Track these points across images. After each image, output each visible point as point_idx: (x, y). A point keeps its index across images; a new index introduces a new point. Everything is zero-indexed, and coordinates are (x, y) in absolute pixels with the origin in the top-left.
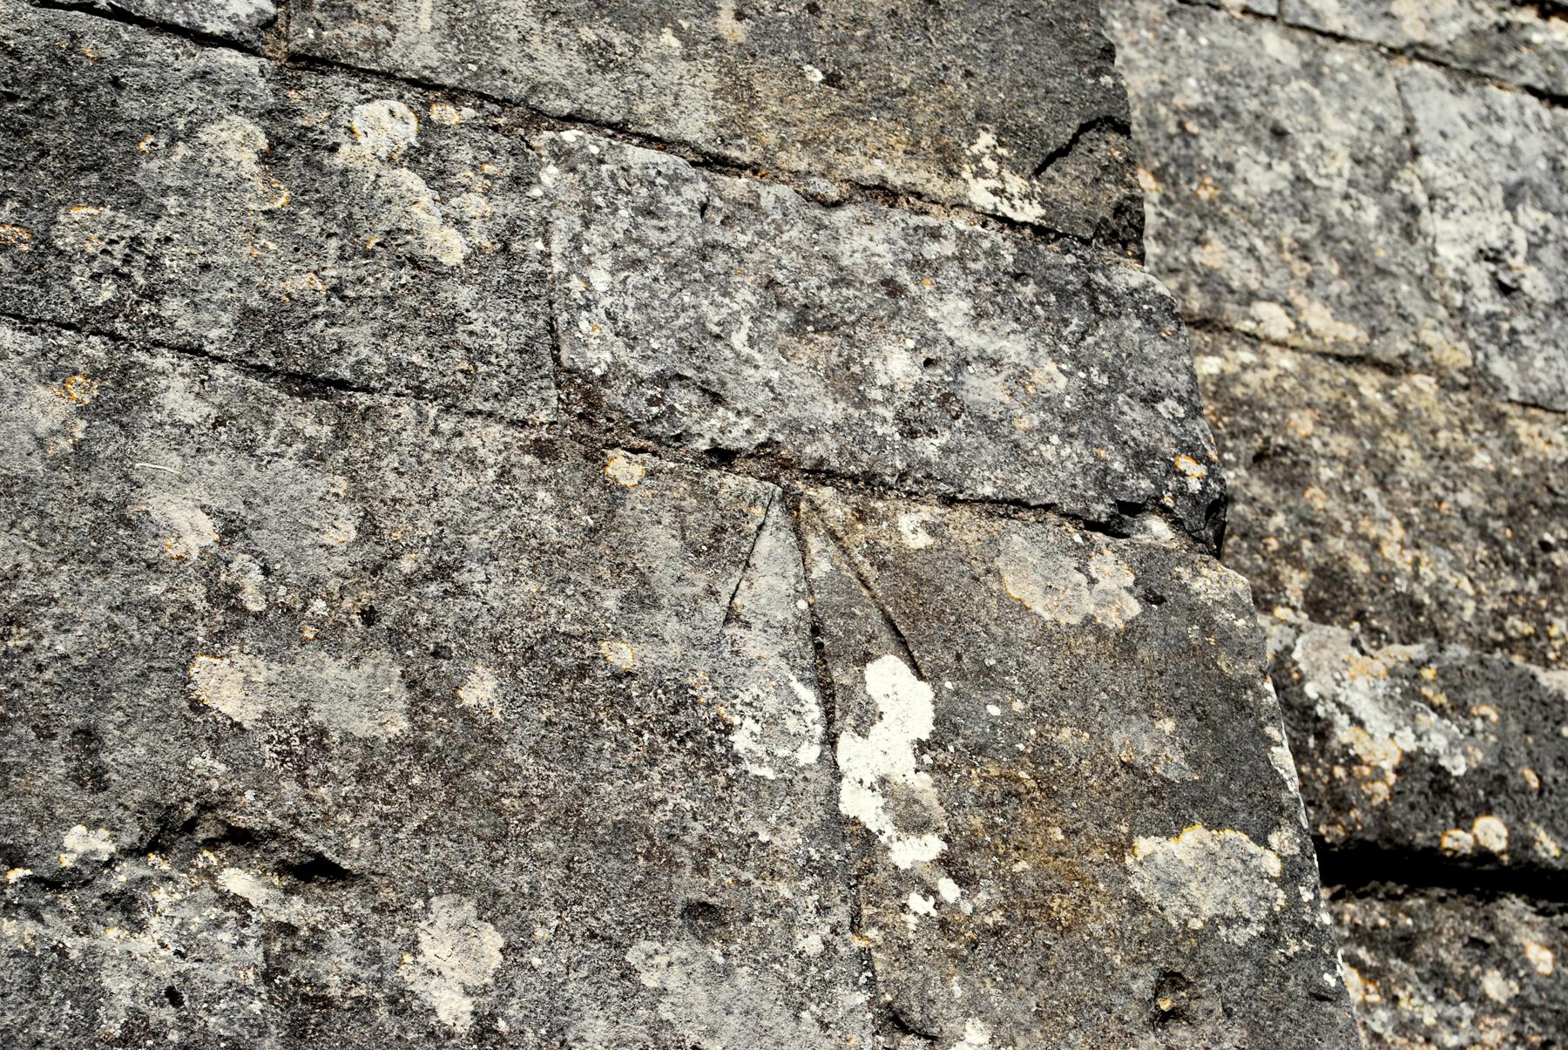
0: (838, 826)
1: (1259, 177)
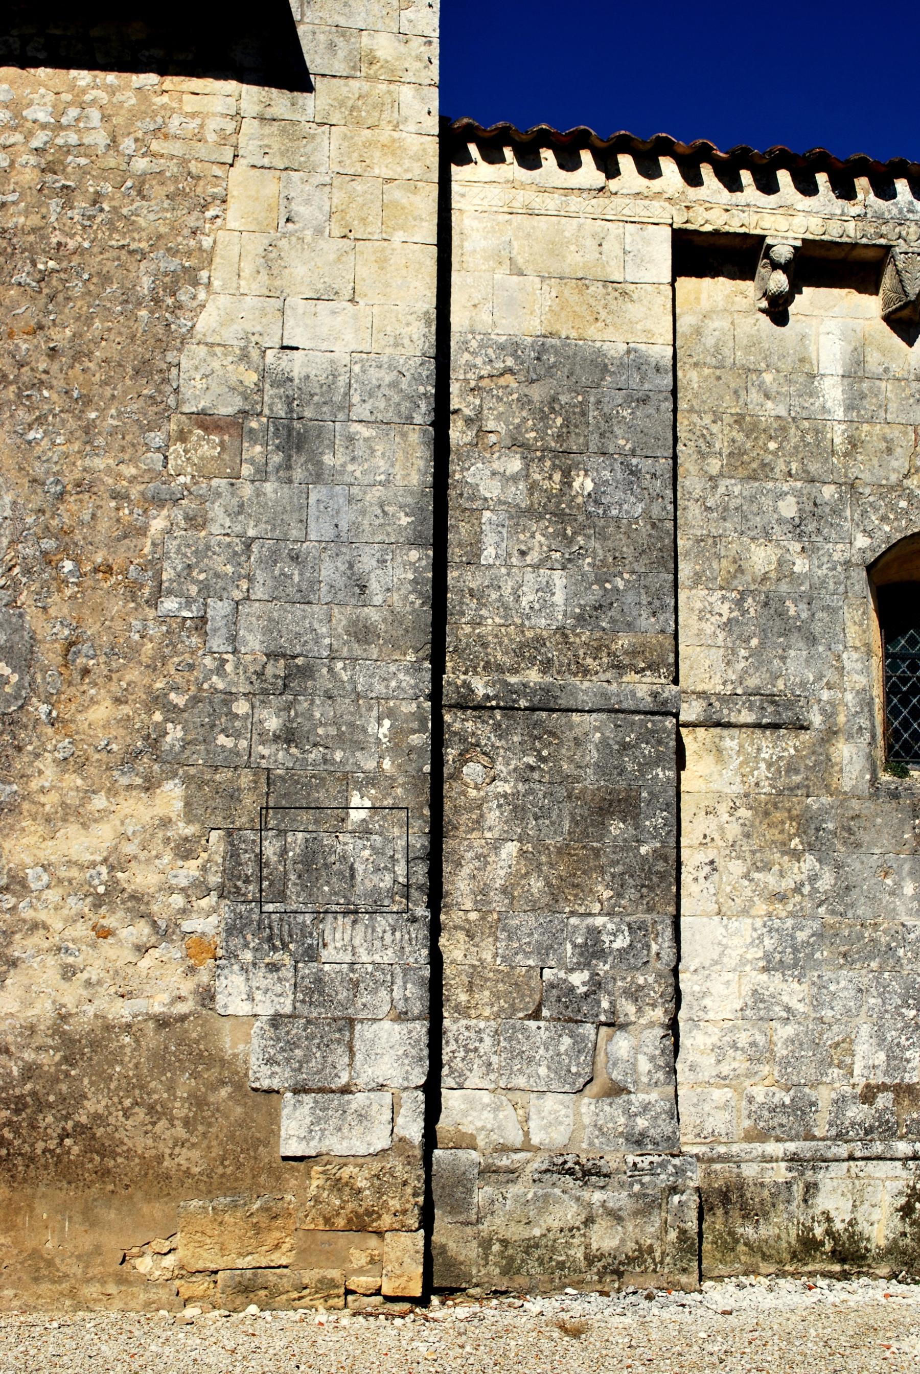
0: (378, 738)
1: (494, 595)
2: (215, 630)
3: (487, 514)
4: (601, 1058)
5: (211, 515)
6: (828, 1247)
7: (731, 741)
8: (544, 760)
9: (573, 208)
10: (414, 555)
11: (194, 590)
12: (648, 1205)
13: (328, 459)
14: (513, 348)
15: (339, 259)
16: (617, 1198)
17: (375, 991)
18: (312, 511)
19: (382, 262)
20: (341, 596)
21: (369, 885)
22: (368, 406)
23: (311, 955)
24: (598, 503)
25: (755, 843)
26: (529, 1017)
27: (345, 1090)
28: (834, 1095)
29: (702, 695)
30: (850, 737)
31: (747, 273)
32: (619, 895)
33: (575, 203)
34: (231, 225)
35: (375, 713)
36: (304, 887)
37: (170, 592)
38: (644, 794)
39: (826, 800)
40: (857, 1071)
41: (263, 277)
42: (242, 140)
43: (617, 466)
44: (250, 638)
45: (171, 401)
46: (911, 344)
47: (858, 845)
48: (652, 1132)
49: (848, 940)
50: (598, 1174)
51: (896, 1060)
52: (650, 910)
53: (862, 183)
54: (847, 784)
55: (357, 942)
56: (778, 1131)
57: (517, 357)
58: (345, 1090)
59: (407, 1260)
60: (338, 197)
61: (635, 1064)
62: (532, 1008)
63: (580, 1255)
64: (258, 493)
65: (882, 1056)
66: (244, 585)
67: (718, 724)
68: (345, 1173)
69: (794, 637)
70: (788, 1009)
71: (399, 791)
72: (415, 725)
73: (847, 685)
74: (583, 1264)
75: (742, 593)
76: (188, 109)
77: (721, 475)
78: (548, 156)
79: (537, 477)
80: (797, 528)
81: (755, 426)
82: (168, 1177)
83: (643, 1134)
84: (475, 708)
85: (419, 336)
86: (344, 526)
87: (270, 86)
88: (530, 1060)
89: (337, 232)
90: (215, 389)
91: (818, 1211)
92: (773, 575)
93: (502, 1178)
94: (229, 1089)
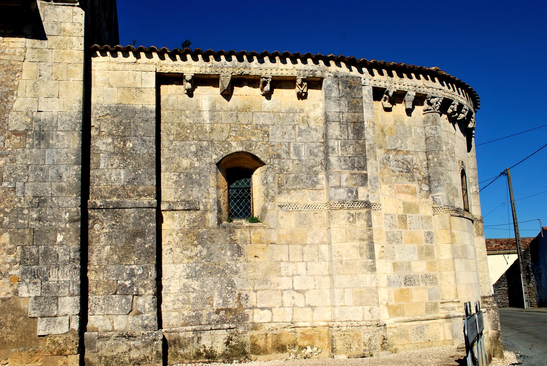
1: (104, 177)
2: (18, 191)
3: (102, 154)
4: (134, 305)
5: (17, 159)
6: (204, 355)
7: (176, 215)
8: (117, 222)
9: (127, 68)
10: (76, 167)
11: (12, 180)
12: (147, 345)
13: (51, 142)
14: (109, 108)
15: (54, 86)
16: (138, 343)
17: (64, 289)
18: (46, 156)
19: (67, 86)
20: (54, 179)
21: (63, 259)
22: (62, 127)
23: (46, 279)
24: (134, 150)
25: (184, 243)
26: (113, 294)
27: (56, 316)
28: (207, 312)
29: (168, 202)
30: (211, 212)
31: (181, 83)
32: (139, 259)
33: (127, 66)
34: (23, 78)
35: (64, 211)
36: (44, 261)
37: (5, 181)
38: (147, 231)
39: (204, 230)
40: (214, 306)
41: (33, 92)
42: (27, 54)
43: (139, 139)
44: (28, 192)
45: (6, 128)
46: (228, 101)
47: (214, 242)
48: (149, 324)
49: (211, 269)
50: (133, 337)
51: (225, 301)
52: (148, 263)
53: (211, 57)
54: (210, 225)
55: (59, 275)
56: (191, 323)
57: (110, 110)
58: (56, 316)
59: (74, 362)
60: (54, 69)
61: (144, 306)
62: (114, 291)
63: (127, 359)
64: (31, 152)
65: (221, 301)
66: (27, 178)
67: (173, 210)
68: (56, 339)
69: (195, 185)
70: (194, 289)
71: (71, 233)
72: (76, 214)
73: (210, 197)
74: (128, 362)
75: (180, 173)
76: (11, 46)
77: (174, 140)
78: (120, 54)
79: (116, 143)
80: (196, 154)
81: (183, 126)
82: (6, 343)
83: (147, 325)
84: (97, 209)
85: (77, 106)
86: (55, 160)
87: (35, 39)
88: (114, 306)
89: (54, 79)
90: (19, 124)
91: (201, 345)
92: (189, 167)
93: (105, 339)
94: (23, 318)
